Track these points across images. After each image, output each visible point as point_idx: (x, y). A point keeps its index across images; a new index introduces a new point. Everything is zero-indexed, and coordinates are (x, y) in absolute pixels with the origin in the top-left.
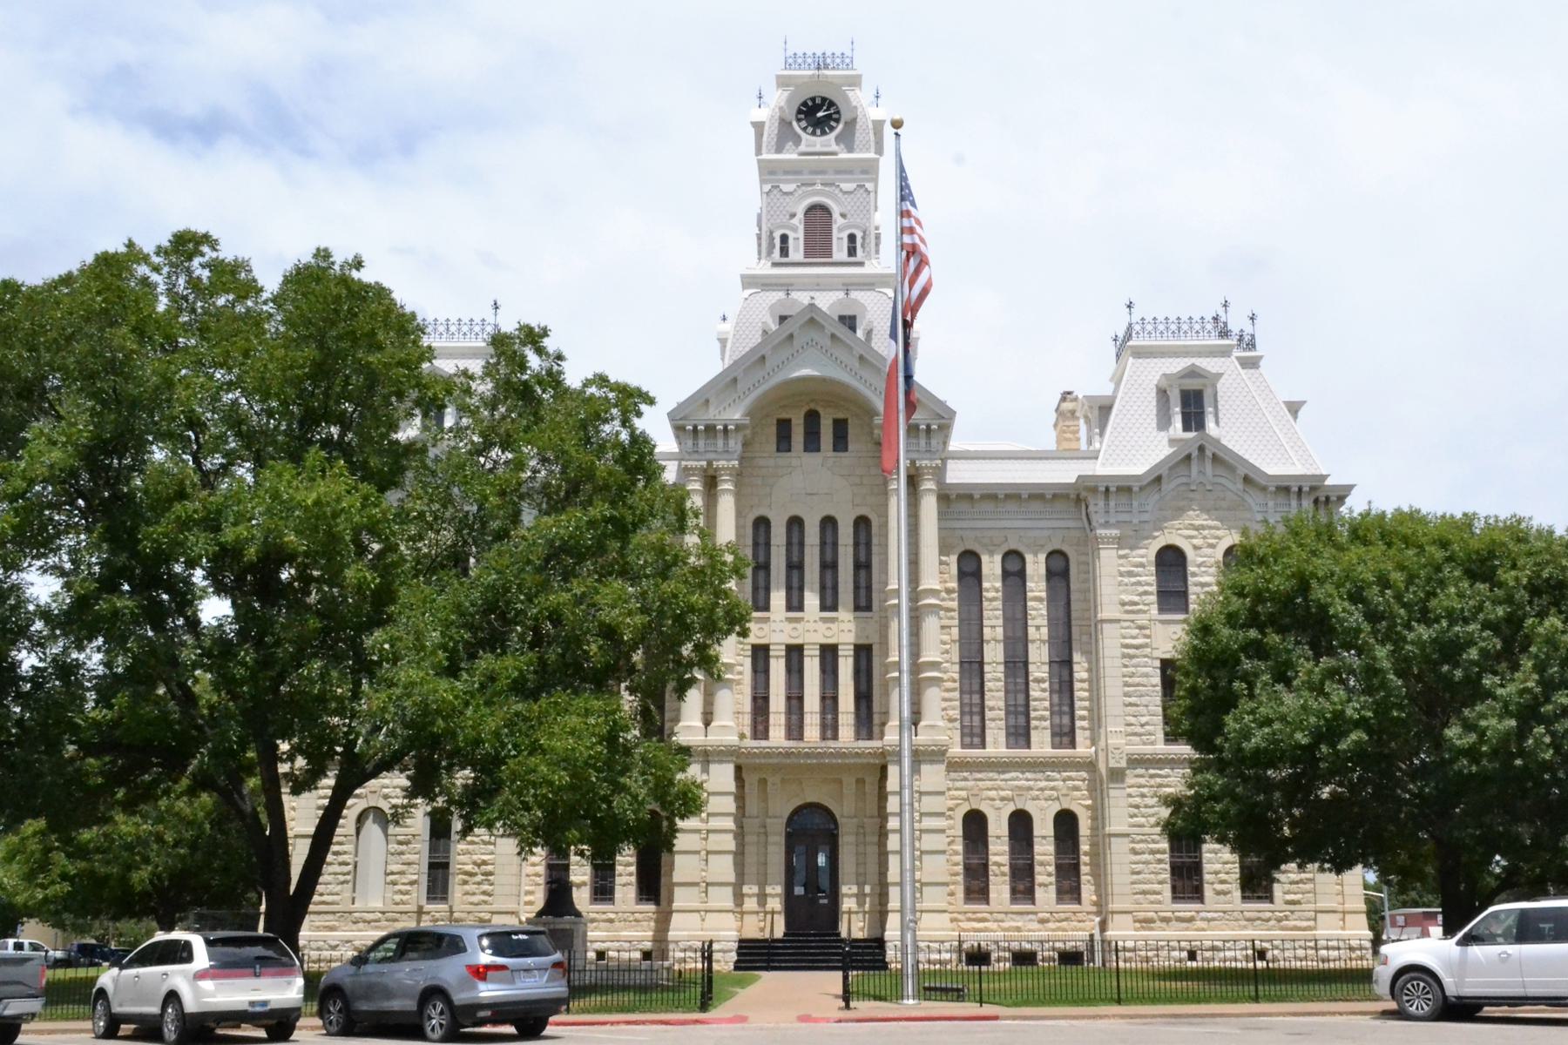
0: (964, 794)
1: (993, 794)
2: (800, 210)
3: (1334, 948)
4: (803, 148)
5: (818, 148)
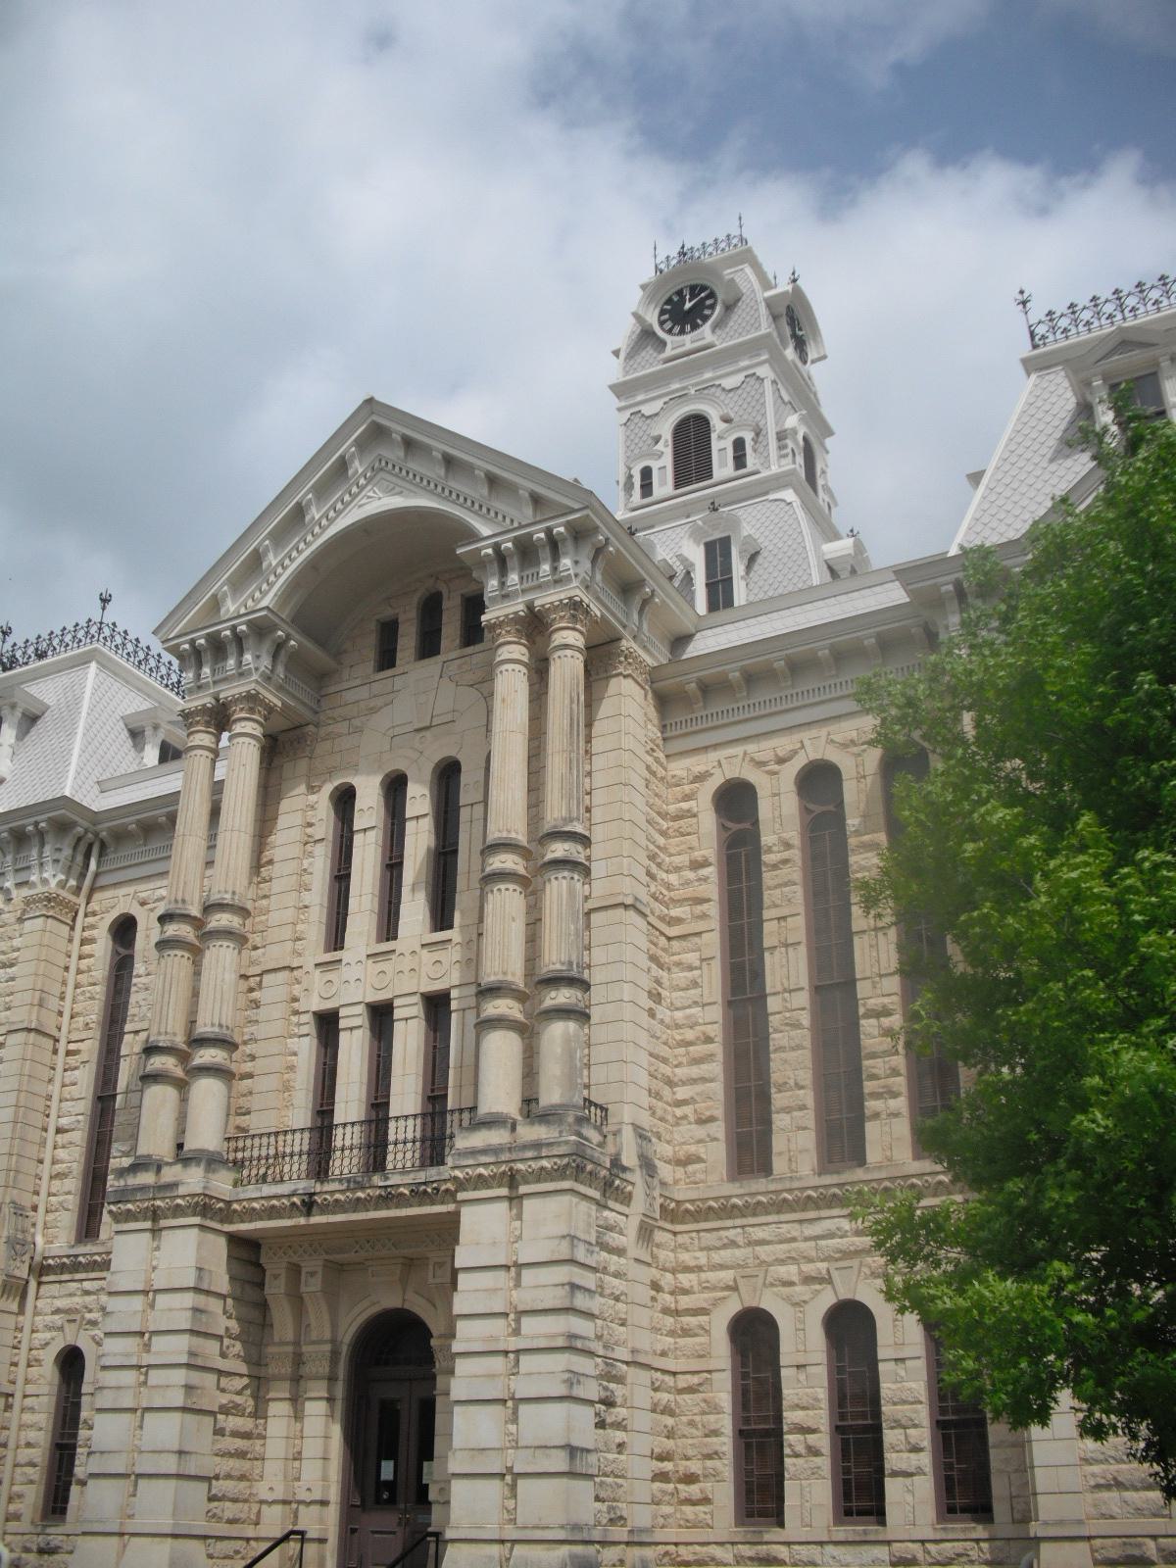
0: (727, 1276)
1: (790, 1271)
2: (666, 429)
3: (688, 1269)
4: (669, 352)
5: (689, 346)
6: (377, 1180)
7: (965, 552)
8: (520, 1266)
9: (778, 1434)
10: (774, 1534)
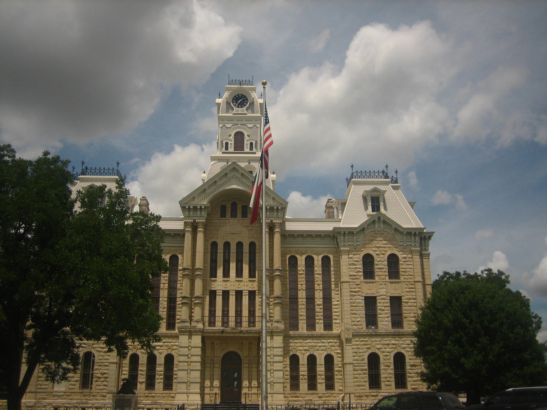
1: (301, 348)
5: (240, 112)
6: (239, 328)
7: (434, 282)
8: (274, 348)
9: (299, 376)
10: (152, 392)
